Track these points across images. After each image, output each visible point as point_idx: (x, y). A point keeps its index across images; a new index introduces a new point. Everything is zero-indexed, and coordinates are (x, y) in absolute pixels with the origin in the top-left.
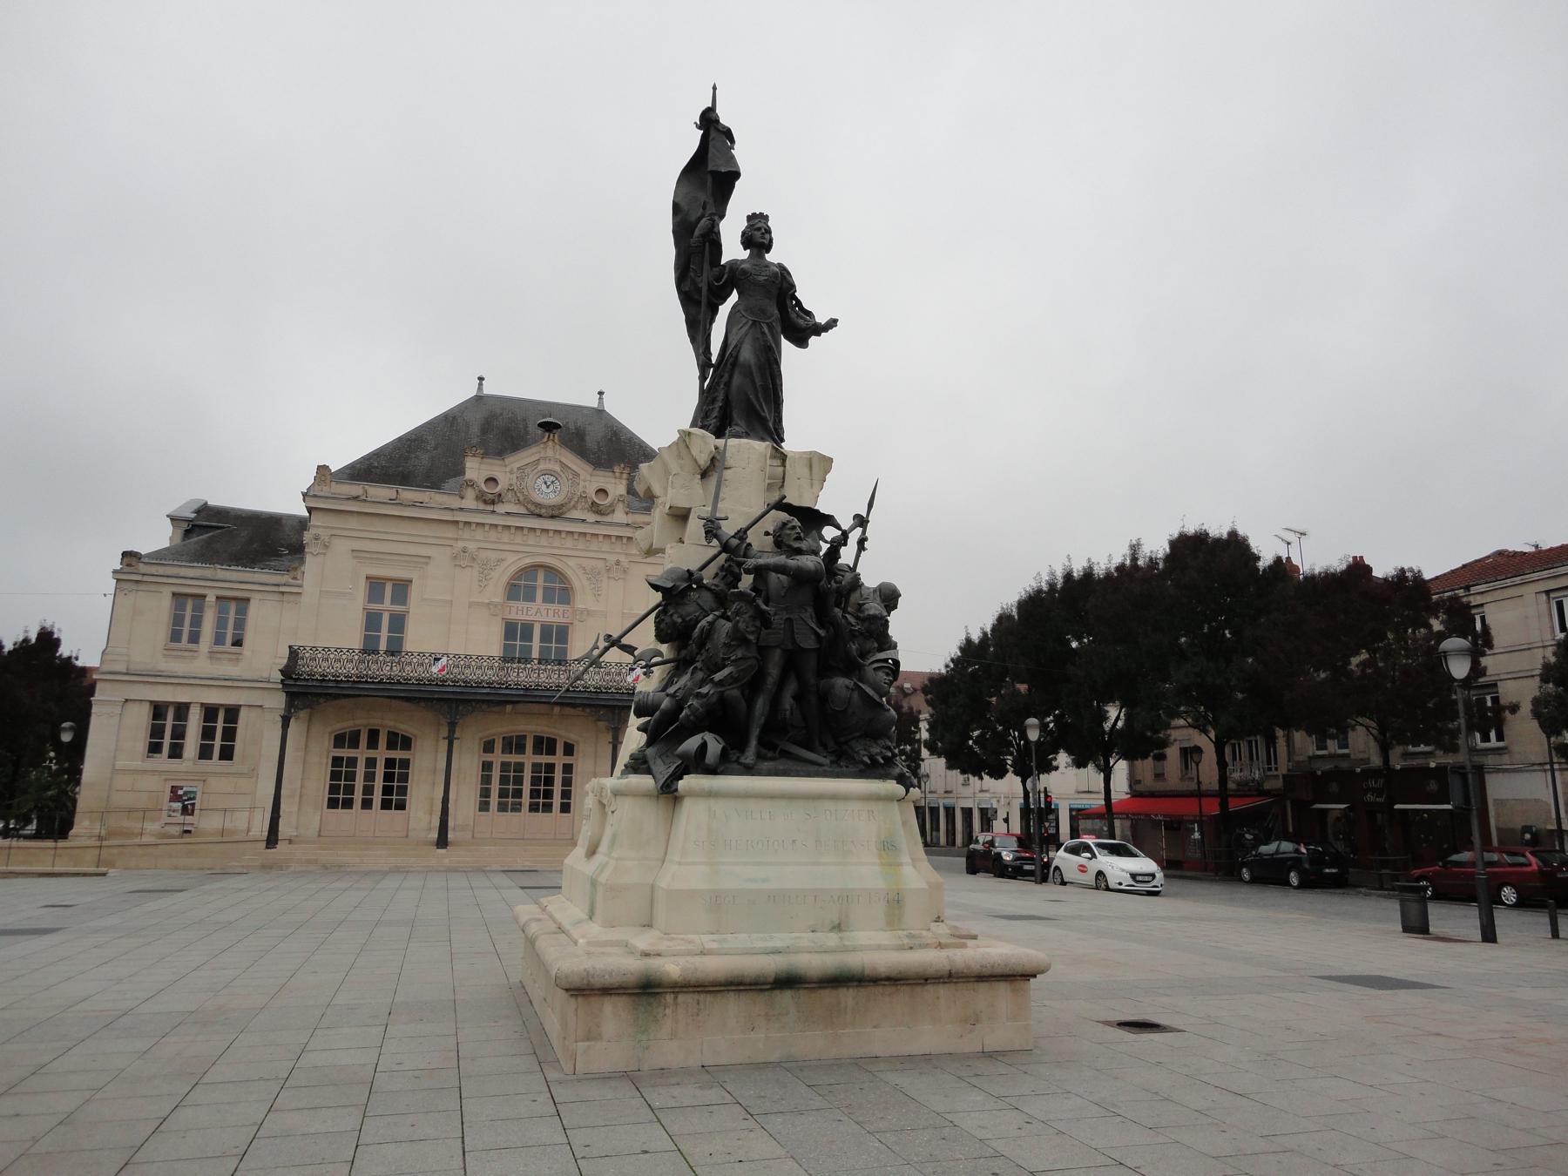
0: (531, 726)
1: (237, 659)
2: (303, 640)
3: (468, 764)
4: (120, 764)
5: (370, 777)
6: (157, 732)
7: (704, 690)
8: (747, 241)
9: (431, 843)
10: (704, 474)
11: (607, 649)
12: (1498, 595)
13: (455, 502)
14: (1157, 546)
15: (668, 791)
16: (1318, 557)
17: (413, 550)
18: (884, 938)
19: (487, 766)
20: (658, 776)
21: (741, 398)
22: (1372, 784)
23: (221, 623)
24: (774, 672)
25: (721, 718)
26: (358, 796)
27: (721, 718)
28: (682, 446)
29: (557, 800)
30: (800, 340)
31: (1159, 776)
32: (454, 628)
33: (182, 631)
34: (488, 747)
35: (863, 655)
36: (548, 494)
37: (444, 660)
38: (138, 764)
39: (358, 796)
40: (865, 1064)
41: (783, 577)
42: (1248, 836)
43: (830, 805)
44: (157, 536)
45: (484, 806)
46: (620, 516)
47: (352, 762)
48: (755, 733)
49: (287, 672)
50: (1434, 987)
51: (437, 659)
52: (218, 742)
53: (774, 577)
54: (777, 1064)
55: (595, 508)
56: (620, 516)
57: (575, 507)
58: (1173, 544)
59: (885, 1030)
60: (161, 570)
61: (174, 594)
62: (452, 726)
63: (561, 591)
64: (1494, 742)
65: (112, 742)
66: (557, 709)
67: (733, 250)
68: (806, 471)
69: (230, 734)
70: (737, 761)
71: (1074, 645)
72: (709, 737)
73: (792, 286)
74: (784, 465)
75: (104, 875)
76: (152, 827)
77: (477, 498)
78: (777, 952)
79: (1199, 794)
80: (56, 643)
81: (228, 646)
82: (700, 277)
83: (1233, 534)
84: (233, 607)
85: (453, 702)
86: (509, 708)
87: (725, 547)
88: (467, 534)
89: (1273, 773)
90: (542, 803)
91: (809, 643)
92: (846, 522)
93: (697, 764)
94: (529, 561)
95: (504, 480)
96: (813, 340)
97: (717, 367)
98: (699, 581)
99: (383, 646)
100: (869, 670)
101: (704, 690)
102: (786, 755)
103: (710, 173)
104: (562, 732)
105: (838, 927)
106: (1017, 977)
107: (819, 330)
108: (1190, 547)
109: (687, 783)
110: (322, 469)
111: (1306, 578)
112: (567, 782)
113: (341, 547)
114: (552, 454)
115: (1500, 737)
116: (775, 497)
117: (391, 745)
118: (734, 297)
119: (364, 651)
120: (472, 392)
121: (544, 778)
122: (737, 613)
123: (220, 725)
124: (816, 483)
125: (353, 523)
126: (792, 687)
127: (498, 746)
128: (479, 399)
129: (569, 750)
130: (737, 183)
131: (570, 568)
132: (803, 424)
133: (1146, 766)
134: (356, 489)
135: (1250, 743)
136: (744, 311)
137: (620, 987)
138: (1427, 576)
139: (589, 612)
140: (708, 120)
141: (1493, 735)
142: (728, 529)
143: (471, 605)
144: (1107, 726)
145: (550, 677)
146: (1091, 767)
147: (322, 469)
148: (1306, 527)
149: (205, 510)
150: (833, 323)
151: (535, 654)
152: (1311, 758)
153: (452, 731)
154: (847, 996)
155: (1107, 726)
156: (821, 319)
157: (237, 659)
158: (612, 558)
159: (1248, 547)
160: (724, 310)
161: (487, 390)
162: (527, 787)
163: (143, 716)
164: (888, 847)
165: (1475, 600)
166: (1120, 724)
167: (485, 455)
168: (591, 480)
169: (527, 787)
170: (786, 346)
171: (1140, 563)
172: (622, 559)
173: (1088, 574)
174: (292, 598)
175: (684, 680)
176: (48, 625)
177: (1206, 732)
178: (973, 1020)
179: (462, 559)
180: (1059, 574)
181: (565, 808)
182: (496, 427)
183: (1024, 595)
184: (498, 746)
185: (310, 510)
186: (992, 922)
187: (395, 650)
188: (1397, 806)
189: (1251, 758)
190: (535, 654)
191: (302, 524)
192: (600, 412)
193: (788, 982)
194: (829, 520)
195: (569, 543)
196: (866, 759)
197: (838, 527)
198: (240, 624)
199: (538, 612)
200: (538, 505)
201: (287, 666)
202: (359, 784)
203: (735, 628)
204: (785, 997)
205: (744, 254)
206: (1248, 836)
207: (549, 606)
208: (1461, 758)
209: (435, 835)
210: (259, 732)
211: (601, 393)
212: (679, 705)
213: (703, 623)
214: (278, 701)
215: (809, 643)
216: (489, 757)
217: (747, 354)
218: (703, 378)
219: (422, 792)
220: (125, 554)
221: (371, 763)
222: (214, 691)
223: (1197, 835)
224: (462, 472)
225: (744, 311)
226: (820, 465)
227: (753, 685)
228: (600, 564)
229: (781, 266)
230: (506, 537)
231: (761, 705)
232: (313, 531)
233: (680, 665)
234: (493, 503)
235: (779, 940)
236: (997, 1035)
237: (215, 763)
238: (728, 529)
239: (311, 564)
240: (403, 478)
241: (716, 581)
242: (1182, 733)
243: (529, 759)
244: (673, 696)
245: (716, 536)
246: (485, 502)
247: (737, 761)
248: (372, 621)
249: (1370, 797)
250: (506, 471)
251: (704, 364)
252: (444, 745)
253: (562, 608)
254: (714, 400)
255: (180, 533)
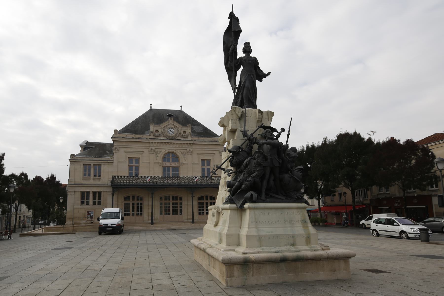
0: (171, 193)
1: (99, 180)
2: (115, 174)
3: (157, 203)
4: (75, 207)
5: (133, 207)
6: (83, 198)
7: (249, 179)
8: (245, 51)
9: (149, 223)
10: (240, 119)
11: (217, 170)
12: (437, 146)
13: (149, 137)
14: (332, 137)
15: (242, 209)
16: (380, 138)
17: (139, 150)
18: (306, 247)
19: (161, 204)
20: (238, 204)
21: (245, 96)
22: (396, 201)
23: (95, 171)
24: (268, 173)
25: (254, 187)
26: (131, 212)
27: (254, 187)
28: (233, 111)
29: (179, 212)
30: (261, 80)
31: (332, 201)
32: (151, 169)
33: (86, 174)
34: (161, 199)
35: (292, 168)
36: (171, 133)
37: (197, 178)
38: (79, 206)
39: (131, 212)
40: (307, 283)
41: (269, 146)
42: (360, 216)
43: (287, 210)
44: (77, 151)
45: (161, 214)
46: (190, 138)
47: (203, 203)
48: (264, 191)
49: (112, 182)
50: (415, 256)
51: (148, 177)
52: (97, 200)
53: (265, 146)
54: (281, 284)
55: (183, 137)
56: (190, 138)
57: (178, 136)
58: (338, 137)
59: (310, 275)
60: (83, 159)
61: (84, 164)
62: (152, 194)
63: (176, 158)
64: (435, 188)
65: (73, 201)
66: (177, 189)
67: (240, 54)
68: (267, 117)
69: (100, 198)
70: (260, 199)
71: (309, 166)
72: (253, 192)
73: (258, 63)
74: (262, 115)
75: (75, 233)
76: (84, 222)
77: (154, 136)
78: (278, 252)
79: (346, 205)
80: (55, 178)
81: (97, 177)
82: (231, 63)
83: (355, 133)
84: (97, 167)
85: (152, 188)
86: (166, 189)
87: (249, 139)
88: (152, 145)
89: (366, 199)
90: (175, 212)
91: (277, 165)
92: (279, 131)
93: (251, 200)
94: (168, 151)
95: (160, 131)
96: (264, 79)
97: (238, 88)
98: (242, 149)
99: (134, 175)
100: (295, 172)
101: (249, 179)
102: (271, 196)
103: (233, 31)
104: (179, 194)
105: (293, 245)
106: (346, 258)
107: (265, 76)
108: (342, 138)
109: (246, 205)
110: (116, 131)
111: (383, 143)
112: (181, 207)
113: (122, 150)
114: (171, 122)
115: (437, 186)
116: (260, 124)
117: (138, 200)
118: (242, 68)
119: (129, 176)
120: (149, 109)
121: (175, 206)
122: (258, 157)
123: (97, 196)
124: (270, 120)
125: (124, 144)
126: (272, 178)
127: (163, 199)
128: (151, 110)
129: (181, 199)
130: (241, 34)
131: (178, 152)
132: (263, 102)
133: (328, 199)
134: (124, 135)
135: (359, 191)
136: (244, 71)
137: (239, 263)
138: (415, 141)
139: (183, 164)
140: (232, 16)
141: (434, 186)
142: (249, 133)
143: (154, 163)
144: (319, 187)
145: (175, 181)
146: (314, 199)
147: (116, 131)
148: (378, 131)
149: (87, 143)
150: (269, 73)
151: (171, 175)
152: (378, 194)
153: (152, 195)
154: (299, 264)
155: (319, 187)
156: (265, 72)
157: (99, 180)
158: (188, 149)
159: (361, 136)
160: (239, 72)
161: (152, 108)
162: (171, 209)
163: (79, 195)
164: (304, 222)
165: (430, 148)
166: (322, 187)
167: (155, 125)
168: (182, 129)
169: (171, 209)
170: (257, 81)
171: (327, 142)
172: (191, 149)
173: (313, 146)
174: (111, 164)
175: (241, 177)
176: (53, 174)
177: (348, 188)
178: (334, 270)
179: (151, 151)
180: (305, 147)
181: (181, 214)
182: (155, 117)
183: (387, 140)
184: (163, 199)
185: (113, 141)
186: (336, 243)
187: (137, 175)
188: (407, 207)
189: (360, 195)
190: (171, 175)
191: (111, 145)
192: (181, 111)
193: (284, 260)
194: (275, 130)
195: (177, 146)
196: (296, 197)
197: (277, 132)
198: (100, 171)
199: (171, 164)
200: (169, 136)
201: (112, 181)
202: (131, 209)
203: (257, 162)
204: (282, 265)
205: (244, 55)
206: (360, 216)
207: (173, 162)
208: (425, 193)
209: (150, 221)
210: (107, 197)
211: (181, 106)
212: (241, 185)
213: (245, 161)
214: (110, 190)
215: (277, 165)
216: (161, 202)
217: (247, 84)
218: (234, 92)
219: (146, 211)
220: (71, 155)
221: (133, 204)
222: (85, 188)
223: (345, 216)
224: (149, 129)
225: (244, 71)
226: (270, 114)
227: (262, 178)
228: (185, 151)
229: (254, 57)
230: (162, 145)
231: (265, 183)
232: (115, 147)
233: (237, 173)
234: (158, 137)
235: (278, 249)
236: (341, 275)
237: (97, 206)
238: (249, 133)
239: (115, 155)
240: (135, 132)
241: (246, 149)
242: (342, 189)
243: (171, 202)
244: (239, 182)
245: (246, 136)
246: (156, 137)
247: (260, 199)
248: (130, 168)
249: (396, 205)
250: (160, 128)
251: (234, 89)
252: (151, 199)
253: (177, 163)
254: (239, 98)
255: (83, 149)
